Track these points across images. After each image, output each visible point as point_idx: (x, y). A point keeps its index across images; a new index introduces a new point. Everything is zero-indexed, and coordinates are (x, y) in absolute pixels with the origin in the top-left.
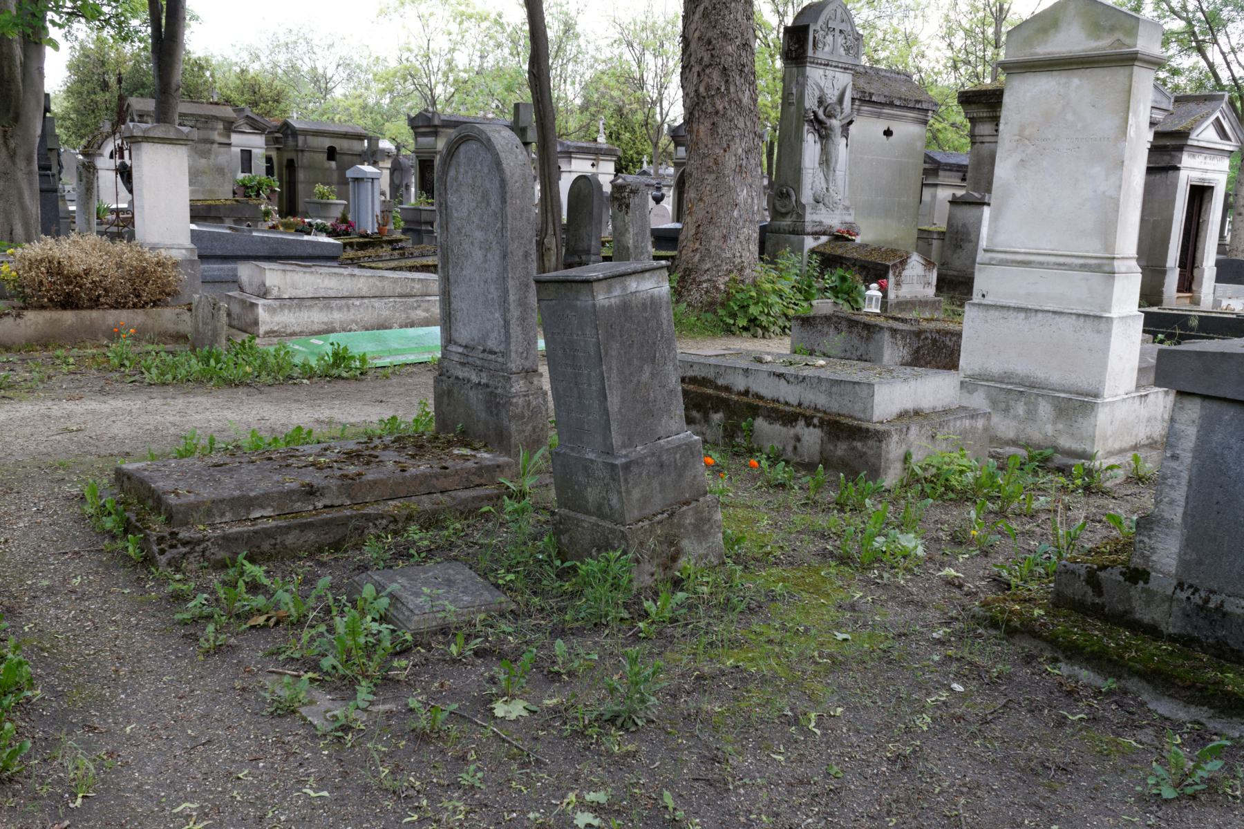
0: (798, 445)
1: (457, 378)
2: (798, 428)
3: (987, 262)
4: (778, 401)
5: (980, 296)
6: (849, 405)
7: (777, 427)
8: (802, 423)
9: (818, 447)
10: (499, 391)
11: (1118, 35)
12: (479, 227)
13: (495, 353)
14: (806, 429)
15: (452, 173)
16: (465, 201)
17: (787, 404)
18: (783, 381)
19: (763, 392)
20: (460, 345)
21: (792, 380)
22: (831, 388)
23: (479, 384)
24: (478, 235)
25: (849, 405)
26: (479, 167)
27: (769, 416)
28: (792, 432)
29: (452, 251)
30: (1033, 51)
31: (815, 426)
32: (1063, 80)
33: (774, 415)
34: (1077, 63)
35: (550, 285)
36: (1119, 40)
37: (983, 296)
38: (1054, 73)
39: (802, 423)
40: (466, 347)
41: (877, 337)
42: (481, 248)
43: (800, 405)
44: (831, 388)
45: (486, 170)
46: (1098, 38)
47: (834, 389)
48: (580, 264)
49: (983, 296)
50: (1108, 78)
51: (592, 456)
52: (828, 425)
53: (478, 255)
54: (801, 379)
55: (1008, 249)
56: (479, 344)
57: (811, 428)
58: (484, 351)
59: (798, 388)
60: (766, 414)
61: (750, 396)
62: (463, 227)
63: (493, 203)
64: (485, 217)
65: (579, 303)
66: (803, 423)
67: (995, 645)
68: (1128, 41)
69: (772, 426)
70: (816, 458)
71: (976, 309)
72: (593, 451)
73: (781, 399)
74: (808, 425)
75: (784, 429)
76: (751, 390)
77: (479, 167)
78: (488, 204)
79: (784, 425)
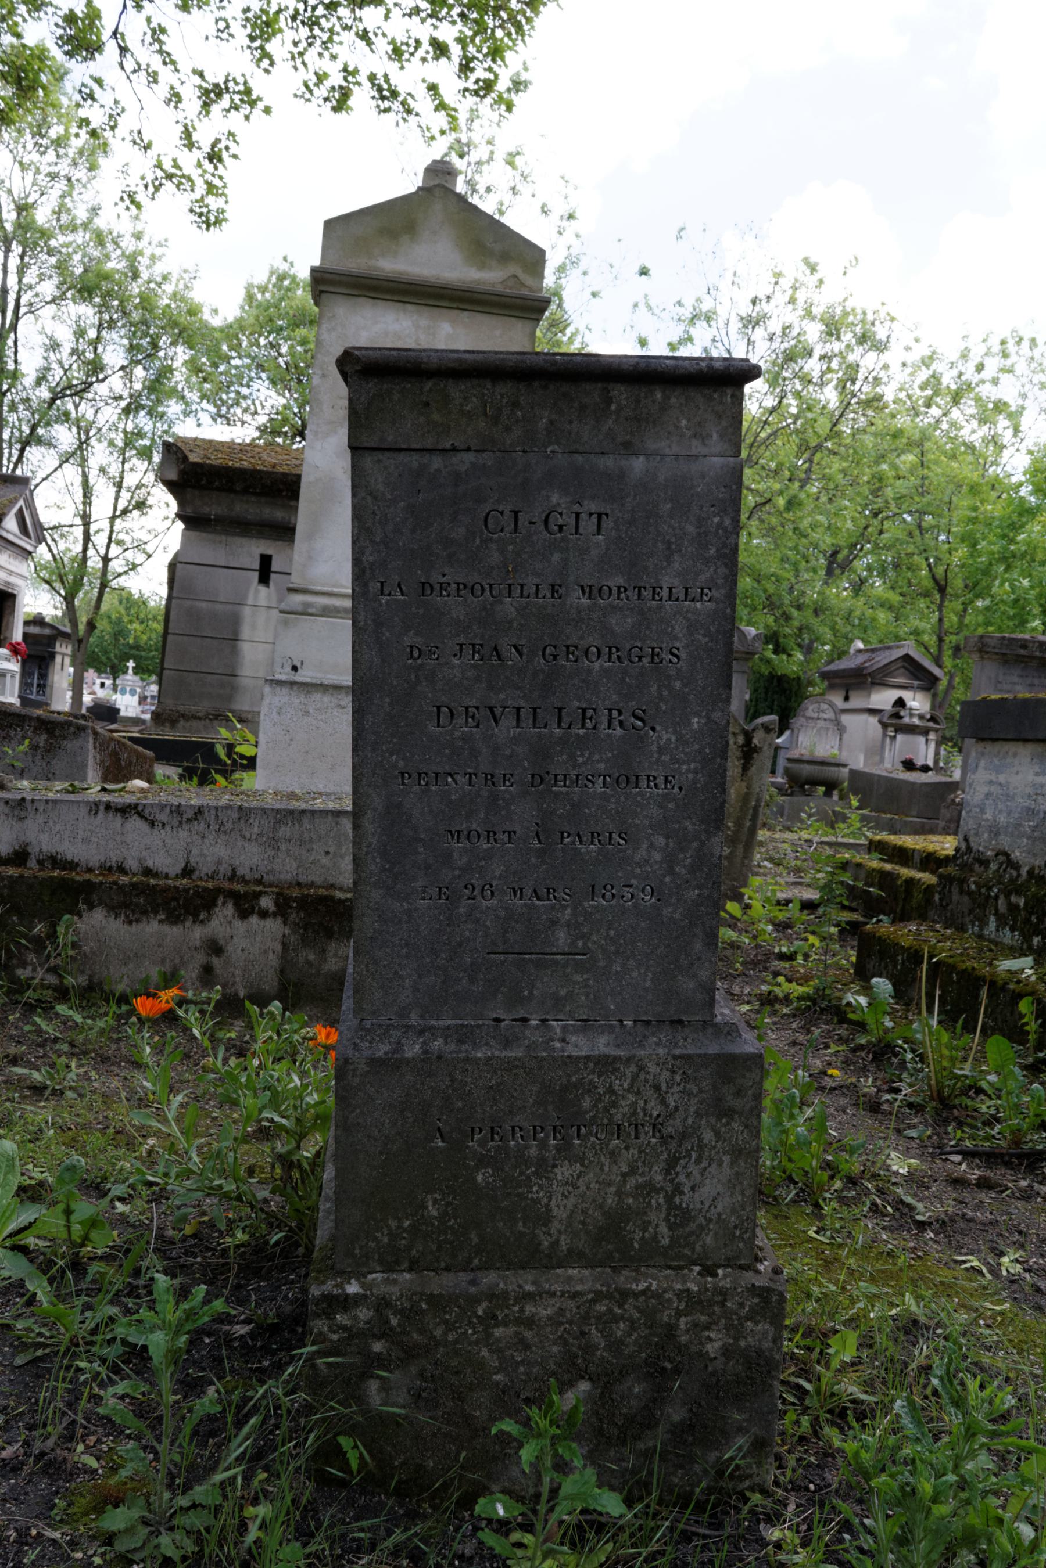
0: (216, 961)
2: (215, 923)
3: (300, 609)
4: (122, 870)
5: (288, 669)
6: (325, 861)
7: (152, 928)
8: (226, 911)
9: (274, 960)
11: (513, 269)
14: (237, 923)
18: (135, 823)
19: (71, 850)
22: (275, 829)
25: (325, 861)
27: (126, 905)
28: (197, 934)
30: (372, 263)
31: (264, 914)
32: (424, 322)
34: (452, 299)
35: (456, 390)
36: (515, 276)
37: (295, 668)
38: (410, 307)
39: (226, 911)
41: (70, 745)
43: (187, 872)
44: (275, 829)
46: (482, 266)
47: (284, 831)
48: (568, 325)
49: (295, 668)
50: (498, 333)
52: (300, 908)
54: (189, 814)
55: (336, 590)
57: (254, 920)
59: (183, 834)
61: (32, 863)
65: (638, 465)
66: (229, 910)
67: (529, 1296)
68: (529, 281)
70: (270, 983)
71: (285, 691)
73: (132, 864)
74: (244, 914)
75: (173, 932)
76: (33, 850)
79: (173, 919)
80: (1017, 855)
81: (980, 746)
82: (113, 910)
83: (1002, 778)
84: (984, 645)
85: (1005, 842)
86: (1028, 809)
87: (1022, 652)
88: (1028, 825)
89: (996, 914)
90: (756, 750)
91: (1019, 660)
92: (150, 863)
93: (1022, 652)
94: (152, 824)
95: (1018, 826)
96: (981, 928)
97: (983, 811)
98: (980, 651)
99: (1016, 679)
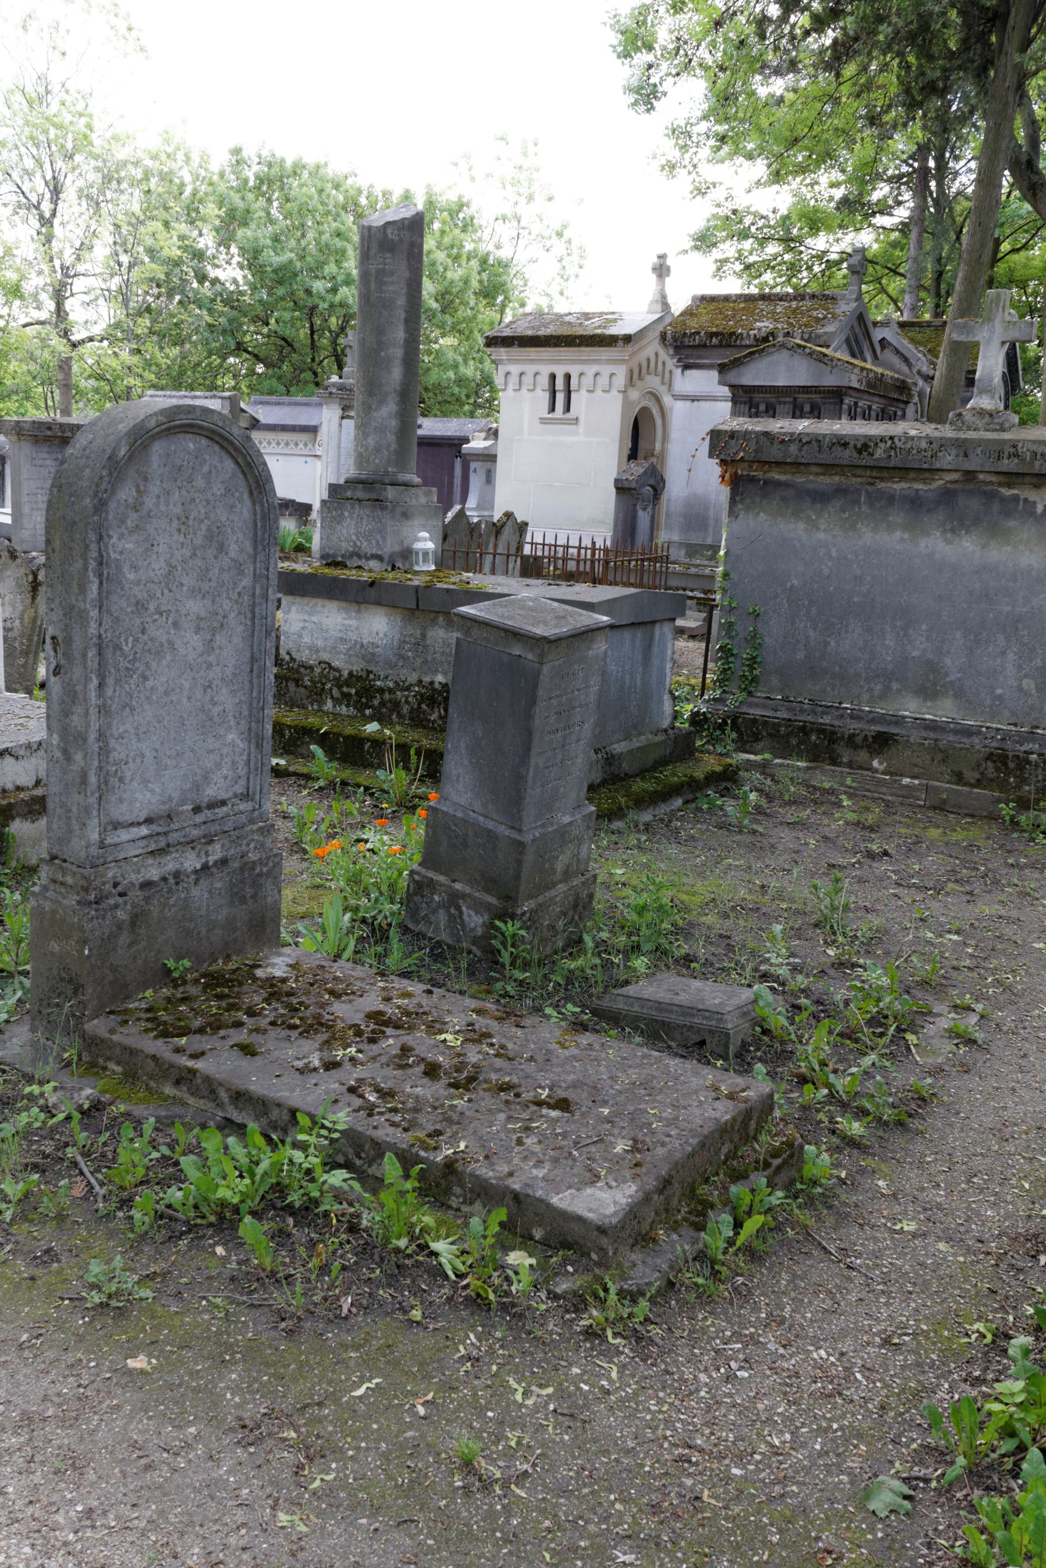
1: (146, 885)
10: (253, 856)
12: (194, 592)
13: (223, 803)
15: (126, 493)
16: (162, 548)
17: (19, 789)
20: (139, 824)
21: (22, 753)
23: (205, 867)
24: (195, 607)
26: (200, 483)
27: (30, 812)
29: (118, 647)
33: (37, 807)
40: (148, 821)
42: (198, 630)
45: (218, 489)
51: (567, 819)
53: (190, 643)
54: (35, 747)
56: (183, 802)
58: (197, 810)
59: (33, 760)
60: (26, 810)
62: (152, 597)
63: (233, 550)
64: (214, 573)
69: (36, 824)
72: (564, 814)
73: (10, 786)
77: (200, 483)
78: (222, 548)
80: (336, 663)
81: (290, 598)
82: (24, 816)
83: (314, 619)
84: (21, 429)
85: (325, 656)
86: (341, 639)
87: (49, 433)
88: (343, 647)
89: (332, 697)
90: (40, 584)
91: (47, 439)
92: (18, 783)
93: (49, 433)
94: (17, 758)
95: (334, 648)
96: (320, 706)
97: (300, 636)
98: (18, 434)
99: (45, 455)
